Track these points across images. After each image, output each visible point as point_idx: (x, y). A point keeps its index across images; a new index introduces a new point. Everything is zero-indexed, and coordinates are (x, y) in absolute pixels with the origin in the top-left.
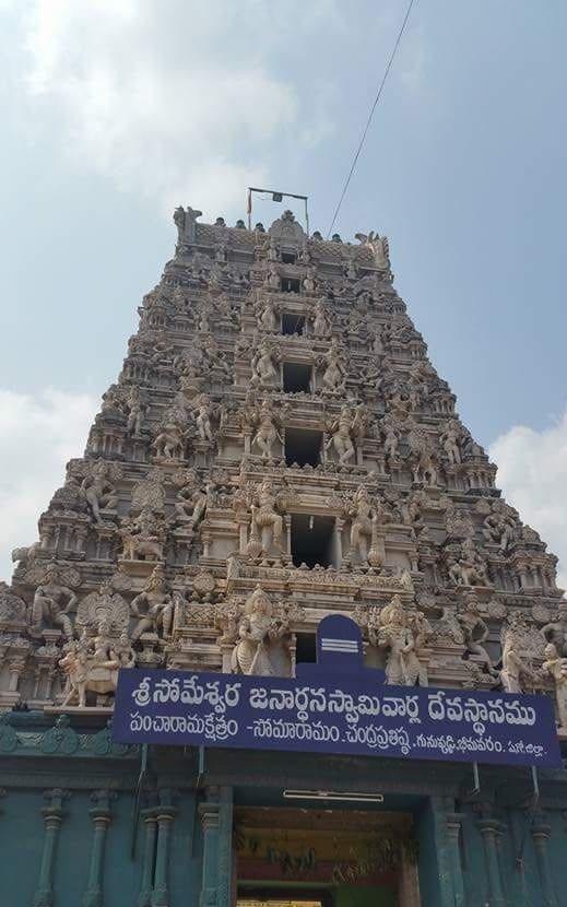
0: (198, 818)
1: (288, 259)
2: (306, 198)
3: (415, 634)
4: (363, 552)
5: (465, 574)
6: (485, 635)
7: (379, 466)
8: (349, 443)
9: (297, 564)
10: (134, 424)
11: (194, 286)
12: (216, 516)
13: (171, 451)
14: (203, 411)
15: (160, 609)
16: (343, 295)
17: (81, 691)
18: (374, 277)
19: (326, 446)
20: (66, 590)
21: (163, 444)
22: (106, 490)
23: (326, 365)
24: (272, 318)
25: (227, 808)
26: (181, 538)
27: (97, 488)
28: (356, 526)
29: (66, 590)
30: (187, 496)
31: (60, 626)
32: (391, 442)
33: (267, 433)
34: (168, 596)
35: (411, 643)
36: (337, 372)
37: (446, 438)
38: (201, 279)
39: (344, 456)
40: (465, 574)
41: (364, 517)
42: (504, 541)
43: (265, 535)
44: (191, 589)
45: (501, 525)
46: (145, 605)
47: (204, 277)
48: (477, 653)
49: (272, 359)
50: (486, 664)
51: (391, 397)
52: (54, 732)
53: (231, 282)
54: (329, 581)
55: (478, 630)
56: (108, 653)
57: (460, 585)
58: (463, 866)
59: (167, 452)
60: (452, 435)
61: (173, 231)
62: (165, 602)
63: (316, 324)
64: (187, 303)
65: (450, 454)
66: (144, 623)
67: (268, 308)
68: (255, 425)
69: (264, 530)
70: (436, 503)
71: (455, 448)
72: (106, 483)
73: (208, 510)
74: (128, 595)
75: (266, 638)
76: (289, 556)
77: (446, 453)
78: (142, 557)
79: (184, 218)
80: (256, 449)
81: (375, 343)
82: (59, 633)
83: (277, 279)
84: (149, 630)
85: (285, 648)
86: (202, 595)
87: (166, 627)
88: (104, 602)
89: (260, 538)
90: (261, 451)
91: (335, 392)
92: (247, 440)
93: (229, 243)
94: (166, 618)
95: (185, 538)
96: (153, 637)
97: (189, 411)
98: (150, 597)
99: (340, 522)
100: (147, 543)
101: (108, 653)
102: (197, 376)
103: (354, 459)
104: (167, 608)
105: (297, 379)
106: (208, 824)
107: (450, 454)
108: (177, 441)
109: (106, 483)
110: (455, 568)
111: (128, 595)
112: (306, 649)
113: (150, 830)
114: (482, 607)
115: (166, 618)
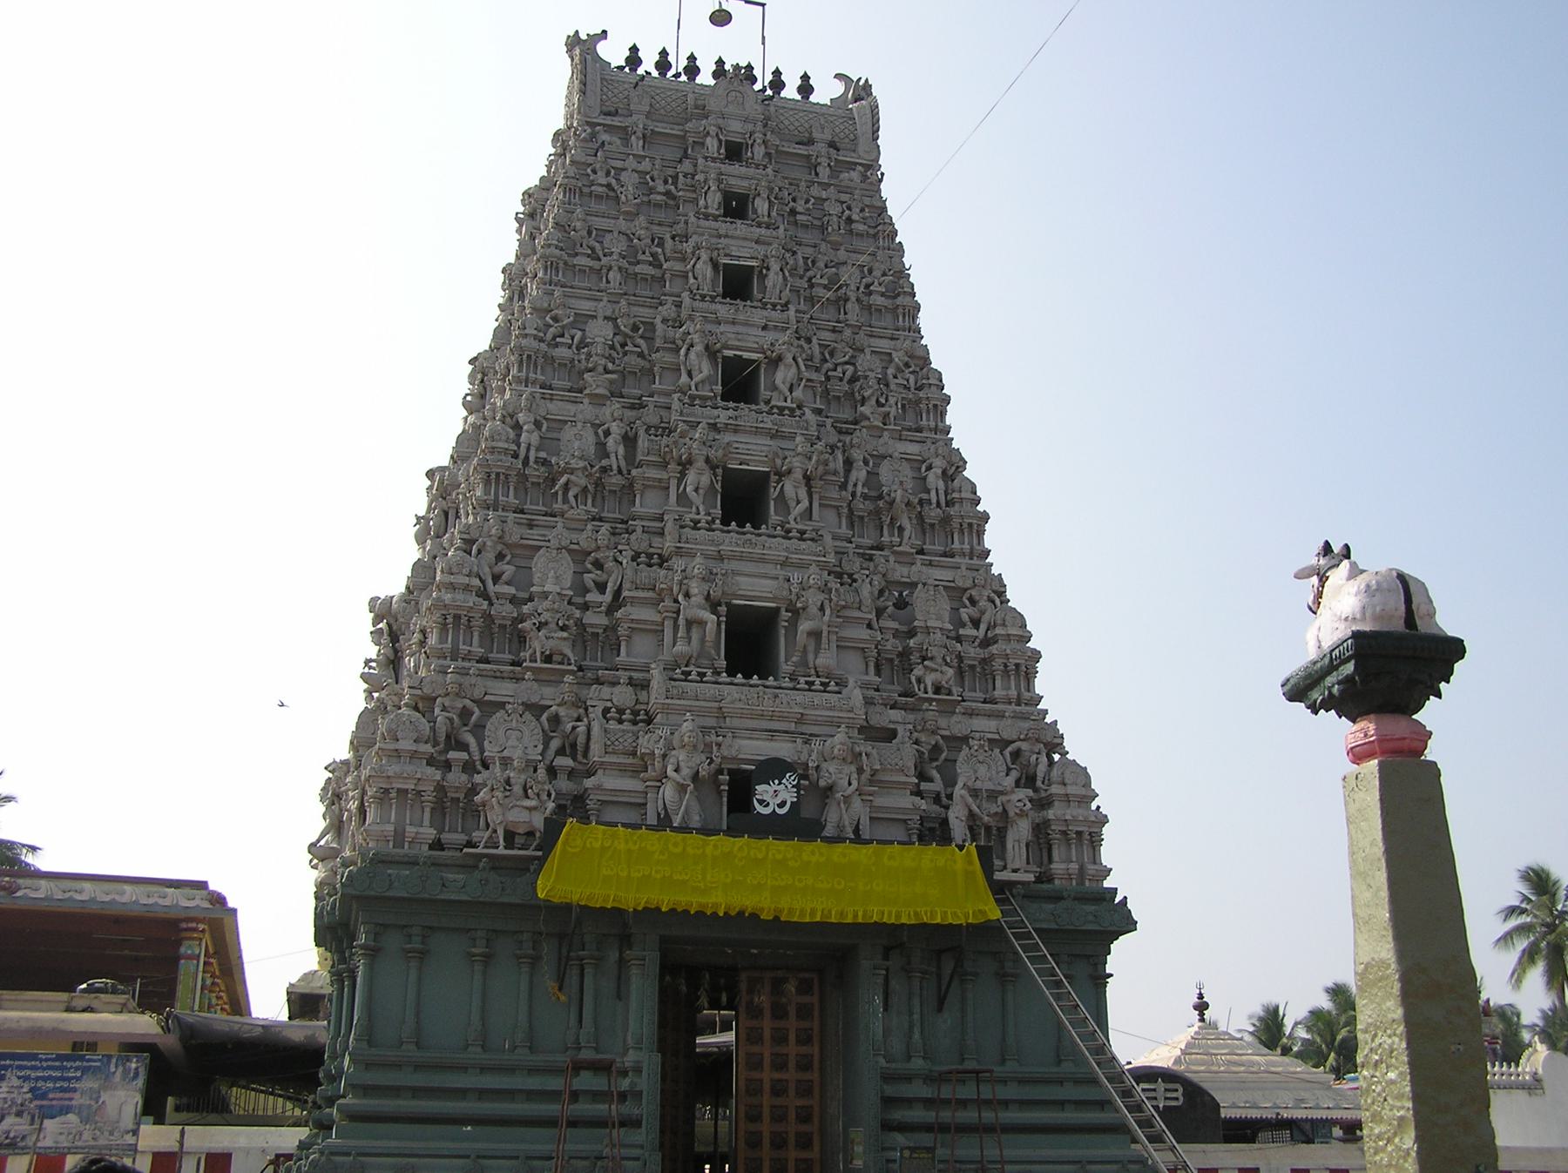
0: (622, 963)
1: (734, 152)
2: (763, 5)
3: (860, 771)
4: (811, 657)
5: (929, 680)
6: (944, 755)
7: (839, 515)
8: (803, 493)
9: (731, 672)
10: (528, 450)
11: (599, 197)
12: (633, 601)
13: (576, 497)
14: (616, 428)
15: (574, 728)
16: (808, 212)
17: (501, 832)
18: (854, 175)
19: (773, 493)
20: (468, 702)
21: (566, 487)
22: (500, 557)
23: (780, 358)
24: (709, 272)
25: (653, 957)
26: (592, 625)
27: (490, 556)
28: (804, 626)
29: (468, 702)
30: (598, 565)
31: (464, 747)
32: (859, 474)
33: (698, 477)
34: (581, 711)
35: (855, 783)
36: (794, 370)
37: (929, 468)
38: (609, 186)
39: (797, 510)
40: (929, 680)
41: (813, 610)
42: (983, 627)
43: (695, 635)
44: (609, 704)
45: (983, 603)
46: (555, 720)
47: (614, 182)
48: (931, 780)
49: (707, 348)
50: (938, 794)
51: (863, 401)
52: (477, 875)
53: (651, 191)
54: (768, 705)
55: (936, 749)
56: (525, 791)
57: (922, 695)
58: (886, 1010)
59: (572, 500)
60: (939, 464)
61: (561, 70)
62: (579, 719)
63: (769, 283)
64: (590, 233)
65: (933, 493)
66: (555, 744)
67: (704, 256)
68: (685, 465)
69: (694, 630)
70: (905, 570)
71: (941, 484)
72: (500, 547)
73: (625, 593)
74: (536, 709)
75: (695, 777)
76: (718, 512)
77: (928, 491)
78: (548, 659)
79: (582, 49)
80: (683, 499)
81: (849, 305)
82: (464, 756)
83: (718, 197)
84: (561, 752)
85: (717, 784)
86: (621, 711)
87: (580, 748)
88: (514, 724)
89: (690, 639)
90: (689, 504)
91: (788, 404)
92: (673, 482)
93: (648, 115)
94: (581, 740)
95: (596, 626)
96: (565, 762)
97: (596, 426)
98: (562, 712)
99: (785, 615)
100: (558, 641)
101: (525, 791)
102: (607, 371)
103: (809, 513)
104: (582, 729)
105: (739, 382)
106: (634, 971)
107: (933, 493)
108: (583, 482)
109: (500, 547)
110: (918, 671)
111: (536, 709)
112: (739, 789)
113: (575, 972)
114: (943, 722)
115: (581, 740)
